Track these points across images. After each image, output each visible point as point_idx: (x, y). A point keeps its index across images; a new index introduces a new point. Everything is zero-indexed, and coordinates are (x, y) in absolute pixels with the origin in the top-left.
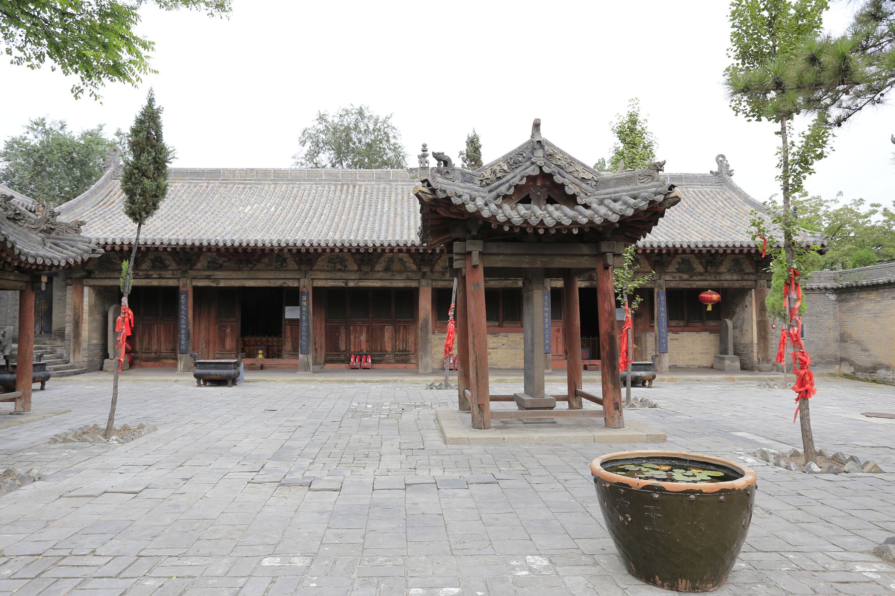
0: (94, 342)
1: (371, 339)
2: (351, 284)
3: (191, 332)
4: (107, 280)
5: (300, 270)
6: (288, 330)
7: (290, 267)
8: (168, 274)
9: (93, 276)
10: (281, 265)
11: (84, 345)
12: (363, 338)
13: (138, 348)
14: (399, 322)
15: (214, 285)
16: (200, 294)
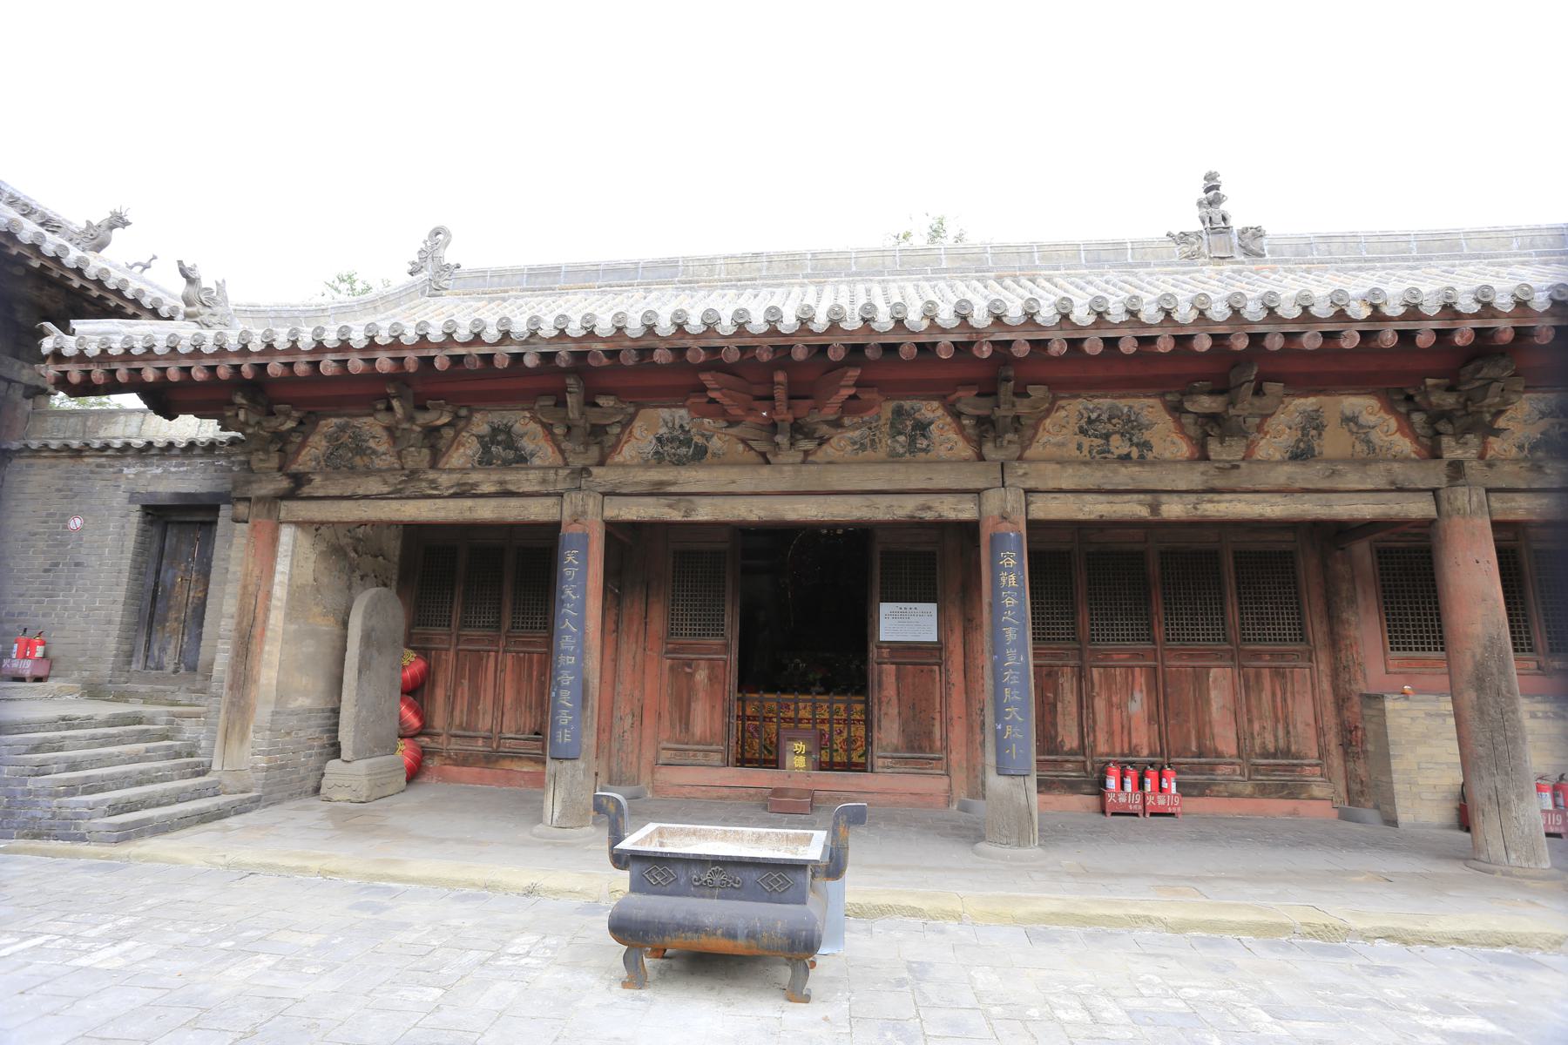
0: (302, 702)
1: (1163, 708)
2: (1173, 509)
3: (595, 681)
4: (345, 504)
5: (981, 458)
6: (886, 679)
7: (943, 452)
8: (526, 480)
9: (306, 490)
10: (912, 446)
11: (262, 713)
12: (1138, 706)
13: (439, 721)
14: (1257, 655)
15: (676, 516)
16: (630, 548)
